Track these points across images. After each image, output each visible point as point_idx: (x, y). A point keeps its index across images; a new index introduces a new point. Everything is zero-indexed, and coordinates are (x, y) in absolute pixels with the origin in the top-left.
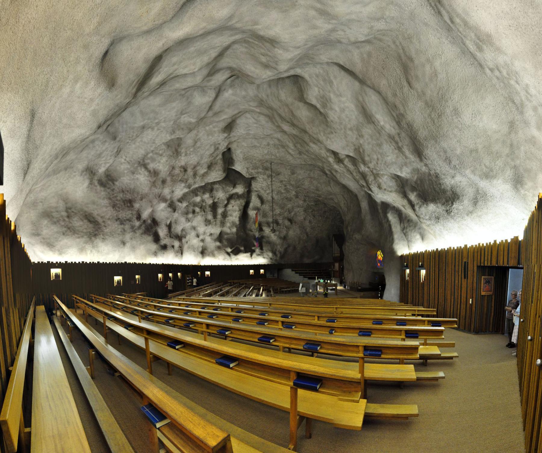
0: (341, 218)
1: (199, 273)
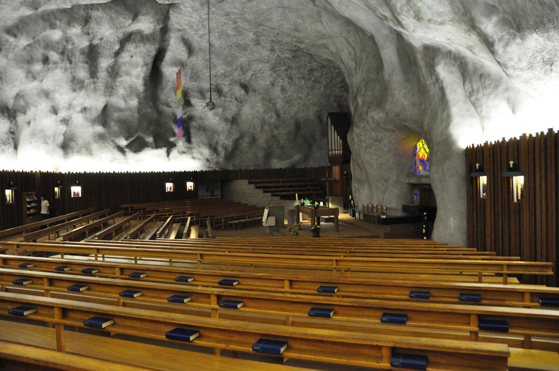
0: (343, 81)
1: (56, 189)
